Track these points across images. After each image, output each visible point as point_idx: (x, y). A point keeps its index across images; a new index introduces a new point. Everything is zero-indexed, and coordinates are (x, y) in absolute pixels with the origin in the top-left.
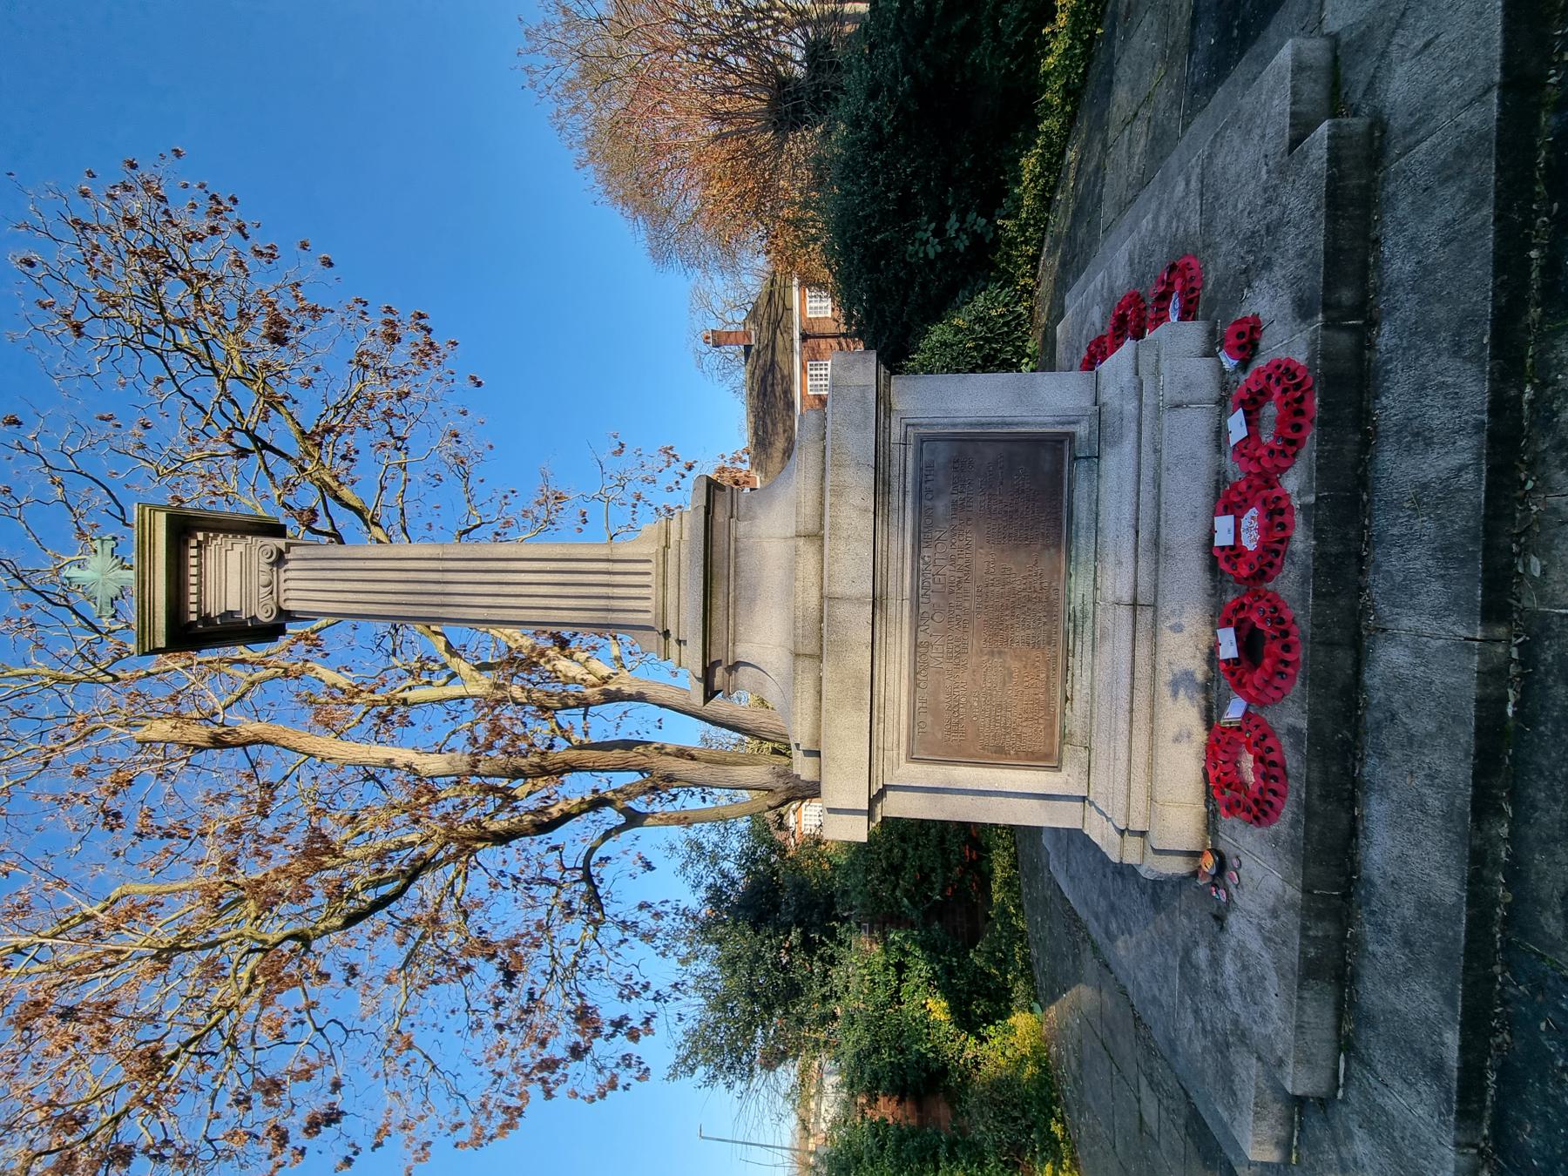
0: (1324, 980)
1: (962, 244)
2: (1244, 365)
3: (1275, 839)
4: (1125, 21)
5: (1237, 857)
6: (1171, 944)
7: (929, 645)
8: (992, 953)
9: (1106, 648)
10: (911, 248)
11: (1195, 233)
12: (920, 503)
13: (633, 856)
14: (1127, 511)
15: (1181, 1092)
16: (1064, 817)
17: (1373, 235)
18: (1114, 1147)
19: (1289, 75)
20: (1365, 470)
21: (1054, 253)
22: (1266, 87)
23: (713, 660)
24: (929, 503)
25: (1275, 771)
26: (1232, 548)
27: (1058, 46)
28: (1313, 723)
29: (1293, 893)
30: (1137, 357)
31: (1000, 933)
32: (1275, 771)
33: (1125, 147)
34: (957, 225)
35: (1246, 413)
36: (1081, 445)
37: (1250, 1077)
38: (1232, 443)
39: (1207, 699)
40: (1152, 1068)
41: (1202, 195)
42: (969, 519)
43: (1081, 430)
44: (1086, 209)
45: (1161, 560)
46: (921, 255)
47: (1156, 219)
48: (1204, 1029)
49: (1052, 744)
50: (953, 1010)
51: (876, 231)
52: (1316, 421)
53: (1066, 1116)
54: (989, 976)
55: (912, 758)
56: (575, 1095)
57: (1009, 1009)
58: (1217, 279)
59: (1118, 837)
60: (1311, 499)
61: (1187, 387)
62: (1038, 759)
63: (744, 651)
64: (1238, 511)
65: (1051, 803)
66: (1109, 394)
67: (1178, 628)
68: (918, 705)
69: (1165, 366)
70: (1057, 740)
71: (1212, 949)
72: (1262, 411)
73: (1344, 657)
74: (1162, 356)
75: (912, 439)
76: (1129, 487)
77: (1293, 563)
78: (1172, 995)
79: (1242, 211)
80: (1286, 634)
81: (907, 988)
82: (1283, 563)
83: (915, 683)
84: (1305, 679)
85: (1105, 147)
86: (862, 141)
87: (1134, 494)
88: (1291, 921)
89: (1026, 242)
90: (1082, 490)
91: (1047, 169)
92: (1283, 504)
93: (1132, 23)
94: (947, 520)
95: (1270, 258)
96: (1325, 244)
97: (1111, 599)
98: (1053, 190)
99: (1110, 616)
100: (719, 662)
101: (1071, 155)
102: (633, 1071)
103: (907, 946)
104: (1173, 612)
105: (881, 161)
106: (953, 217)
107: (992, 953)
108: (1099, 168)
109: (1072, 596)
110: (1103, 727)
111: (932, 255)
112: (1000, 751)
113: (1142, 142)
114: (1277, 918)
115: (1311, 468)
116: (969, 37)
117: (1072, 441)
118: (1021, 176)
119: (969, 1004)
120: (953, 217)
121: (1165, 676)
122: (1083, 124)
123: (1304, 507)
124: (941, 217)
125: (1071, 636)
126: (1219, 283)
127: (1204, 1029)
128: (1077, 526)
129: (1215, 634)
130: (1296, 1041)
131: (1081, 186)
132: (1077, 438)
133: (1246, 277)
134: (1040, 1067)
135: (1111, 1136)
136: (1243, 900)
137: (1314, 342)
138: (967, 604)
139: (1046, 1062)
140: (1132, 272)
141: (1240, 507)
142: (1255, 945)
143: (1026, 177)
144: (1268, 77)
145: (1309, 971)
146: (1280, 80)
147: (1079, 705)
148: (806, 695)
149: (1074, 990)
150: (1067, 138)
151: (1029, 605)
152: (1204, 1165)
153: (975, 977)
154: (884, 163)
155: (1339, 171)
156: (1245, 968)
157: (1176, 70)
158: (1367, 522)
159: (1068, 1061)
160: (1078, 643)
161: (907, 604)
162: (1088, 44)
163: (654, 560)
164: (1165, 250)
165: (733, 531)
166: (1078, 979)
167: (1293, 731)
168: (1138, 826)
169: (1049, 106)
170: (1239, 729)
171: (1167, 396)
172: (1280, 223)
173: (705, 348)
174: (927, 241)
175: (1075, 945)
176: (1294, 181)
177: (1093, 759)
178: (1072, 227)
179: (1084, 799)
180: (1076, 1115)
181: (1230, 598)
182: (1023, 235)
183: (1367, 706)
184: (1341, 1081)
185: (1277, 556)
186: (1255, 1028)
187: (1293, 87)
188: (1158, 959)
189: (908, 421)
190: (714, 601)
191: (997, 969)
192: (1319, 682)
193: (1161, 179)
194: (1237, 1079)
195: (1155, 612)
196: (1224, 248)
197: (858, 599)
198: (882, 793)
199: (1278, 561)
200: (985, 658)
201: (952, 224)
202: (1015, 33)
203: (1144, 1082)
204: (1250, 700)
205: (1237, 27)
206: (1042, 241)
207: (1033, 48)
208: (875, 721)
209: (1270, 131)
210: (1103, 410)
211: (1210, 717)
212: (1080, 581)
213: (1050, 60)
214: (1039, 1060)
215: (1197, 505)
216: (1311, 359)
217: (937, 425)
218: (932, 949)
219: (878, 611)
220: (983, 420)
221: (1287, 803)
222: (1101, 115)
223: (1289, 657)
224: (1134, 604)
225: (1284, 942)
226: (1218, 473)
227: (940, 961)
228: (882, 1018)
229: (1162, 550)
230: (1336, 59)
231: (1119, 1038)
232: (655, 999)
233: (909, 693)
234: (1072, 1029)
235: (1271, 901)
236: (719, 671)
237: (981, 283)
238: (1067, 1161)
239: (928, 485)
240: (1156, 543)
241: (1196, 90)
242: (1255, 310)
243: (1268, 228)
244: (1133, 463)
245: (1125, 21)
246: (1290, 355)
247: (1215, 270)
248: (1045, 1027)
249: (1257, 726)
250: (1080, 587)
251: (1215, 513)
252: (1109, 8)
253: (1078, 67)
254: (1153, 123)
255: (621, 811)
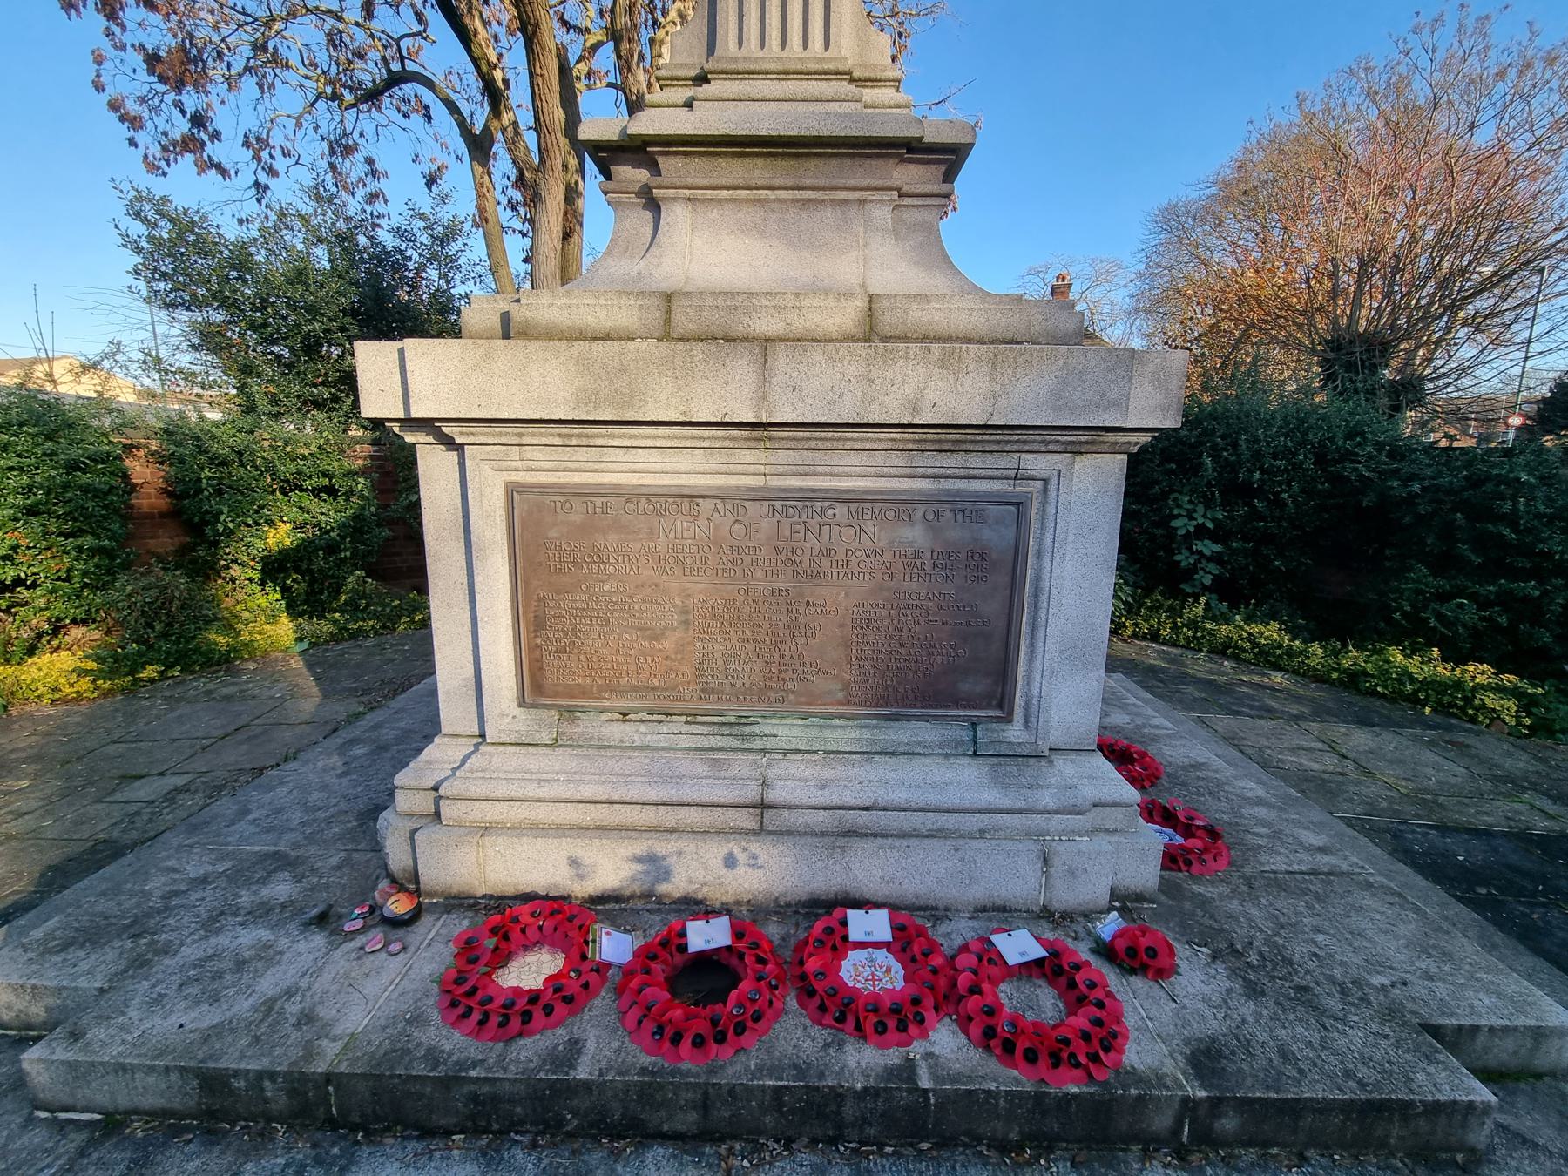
0: (200, 1097)
1: (1183, 559)
2: (1107, 951)
3: (417, 1020)
4: (1447, 742)
5: (404, 949)
6: (310, 839)
7: (695, 517)
8: (364, 596)
9: (701, 769)
10: (1186, 499)
11: (1261, 864)
12: (920, 502)
13: (442, 158)
14: (899, 796)
15: (152, 833)
16: (454, 711)
17: (1311, 1153)
18: (114, 742)
19: (1533, 1023)
20: (965, 1145)
21: (1163, 659)
22: (1498, 979)
23: (661, 160)
24: (919, 514)
25: (515, 1023)
26: (845, 938)
27: (1414, 666)
28: (587, 1086)
29: (329, 1057)
30: (1115, 804)
31: (388, 605)
32: (515, 1023)
33: (1304, 744)
34: (1207, 552)
35: (1039, 962)
36: (993, 731)
37: (74, 977)
38: (994, 938)
39: (632, 897)
40: (196, 791)
41: (1314, 873)
42: (891, 576)
43: (1015, 732)
44: (1217, 696)
45: (827, 840)
46: (1176, 512)
47: (1259, 802)
48: (176, 894)
49: (557, 695)
50: (284, 553)
51: (1216, 457)
52: (1044, 1089)
53: (170, 681)
54: (336, 594)
55: (512, 490)
56: (99, 60)
57: (301, 615)
58: (1210, 901)
59: (431, 784)
60: (925, 1082)
61: (1072, 873)
62: (532, 676)
63: (677, 216)
64: (898, 946)
65: (473, 693)
66: (1065, 768)
67: (730, 862)
68: (598, 501)
69: (1102, 843)
70: (564, 702)
71: (283, 906)
72: (1041, 982)
73: (687, 1120)
74: (1115, 839)
75: (1022, 487)
76: (932, 798)
77: (827, 1046)
78: (240, 841)
79: (1314, 942)
80: (721, 1039)
81: (307, 500)
82: (824, 1026)
83: (630, 496)
84: (652, 1073)
85: (1297, 719)
86: (1332, 439)
87: (922, 804)
88: (283, 1056)
89: (1175, 628)
90: (927, 733)
91: (1261, 652)
92: (913, 1029)
93: (1445, 749)
94: (891, 543)
95: (1263, 994)
96: (1312, 1099)
97: (772, 773)
98: (1236, 657)
99: (746, 772)
100: (655, 169)
101: (1277, 678)
102: (155, 150)
103: (353, 499)
104: (754, 857)
105: (1302, 462)
106: (1217, 548)
107: (364, 596)
108: (1270, 713)
109: (774, 721)
110: (586, 764)
111: (1174, 523)
112: (539, 624)
113: (1316, 766)
114: (298, 1025)
115: (971, 1079)
116: (1444, 563)
117: (999, 720)
118: (1256, 622)
119: (297, 570)
120: (1217, 548)
121: (661, 847)
122: (1314, 691)
123: (909, 1067)
124: (1219, 534)
125: (715, 719)
126: (1204, 902)
127: (176, 894)
128: (876, 727)
129: (725, 910)
130: (101, 1063)
131: (1245, 690)
132: (1003, 726)
133: (1226, 952)
134: (229, 652)
135: (128, 738)
136: (342, 959)
137: (1160, 1081)
138: (759, 574)
139: (235, 658)
140: (1184, 768)
141: (904, 950)
142: (268, 984)
143: (1255, 629)
144: (1515, 984)
145: (213, 1082)
146: (1521, 1005)
147: (618, 731)
148: (602, 314)
149: (316, 690)
150: (1295, 672)
151: (760, 663)
152: (50, 868)
153: (332, 577)
154: (1298, 466)
155: (1419, 1115)
156: (240, 964)
157: (1410, 809)
158: (889, 1150)
159: (234, 684)
160: (706, 729)
161: (758, 481)
162: (1413, 699)
163: (827, 54)
164: (1225, 817)
165: (877, 196)
166: (326, 695)
167: (575, 1046)
168: (447, 810)
169: (1336, 654)
170: (584, 957)
171: (1060, 848)
172: (1317, 1010)
173: (1051, 279)
174: (1191, 518)
175: (366, 692)
176: (1386, 1037)
177: (541, 750)
178: (1198, 681)
179: (483, 736)
180: (167, 694)
181: (773, 930)
182: (1184, 625)
183: (616, 1155)
184: (63, 1116)
185: (837, 1020)
186: (146, 984)
187: (1516, 1028)
188: (297, 817)
189: (1054, 481)
190: (760, 161)
191: (346, 602)
192: (648, 1092)
193: (1290, 797)
194: (81, 954)
195: (754, 833)
196: (1255, 912)
197: (765, 398)
198: (449, 443)
199: (828, 1020)
200: (678, 602)
201: (1208, 547)
202: (1440, 617)
203: (180, 781)
204: (628, 971)
205: (1489, 893)
206: (1174, 644)
207: (1415, 636)
208: (564, 430)
209: (1441, 989)
210: (1043, 762)
211: (608, 905)
212: (796, 732)
213: (1400, 657)
214: (236, 650)
215: (905, 886)
216: (1134, 1077)
217: (1042, 529)
218: (356, 527)
219: (744, 433)
220: (1044, 598)
221: (467, 1040)
222: (1329, 712)
223: (686, 1044)
224: (763, 806)
225: (257, 1039)
226: (947, 909)
227: (343, 538)
228: (257, 469)
229: (842, 842)
230: (1538, 1076)
231: (245, 747)
232: (257, 184)
233: (616, 486)
234: (270, 688)
235: (325, 1012)
236: (641, 175)
237: (1131, 579)
238: (107, 685)
239: (948, 514)
240: (851, 833)
241: (1394, 836)
242: (1183, 966)
243: (1306, 989)
244: (967, 804)
245: (1447, 742)
246: (1133, 1035)
247: (1222, 897)
248: (280, 656)
249: (586, 986)
250: (786, 731)
251: (893, 908)
252: (1454, 721)
253: (1385, 687)
254: (1340, 778)
255: (486, 128)
